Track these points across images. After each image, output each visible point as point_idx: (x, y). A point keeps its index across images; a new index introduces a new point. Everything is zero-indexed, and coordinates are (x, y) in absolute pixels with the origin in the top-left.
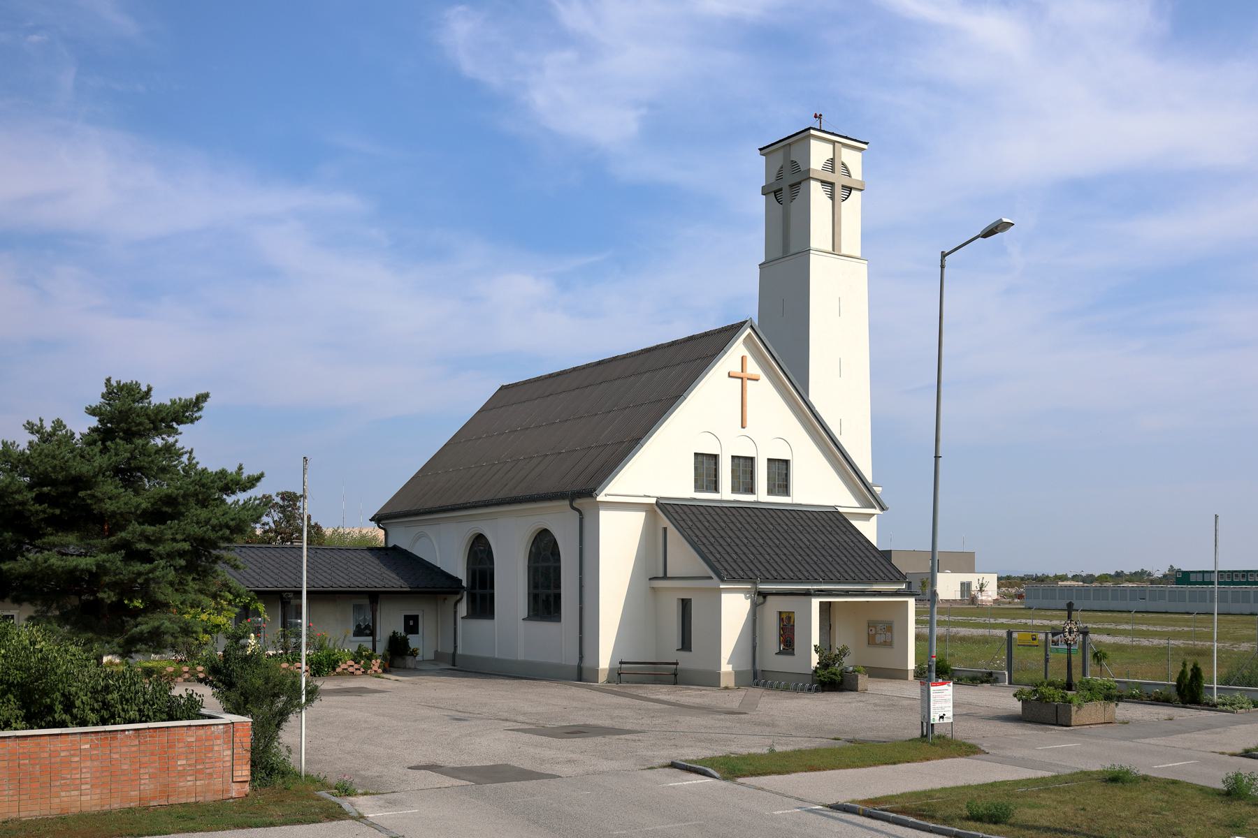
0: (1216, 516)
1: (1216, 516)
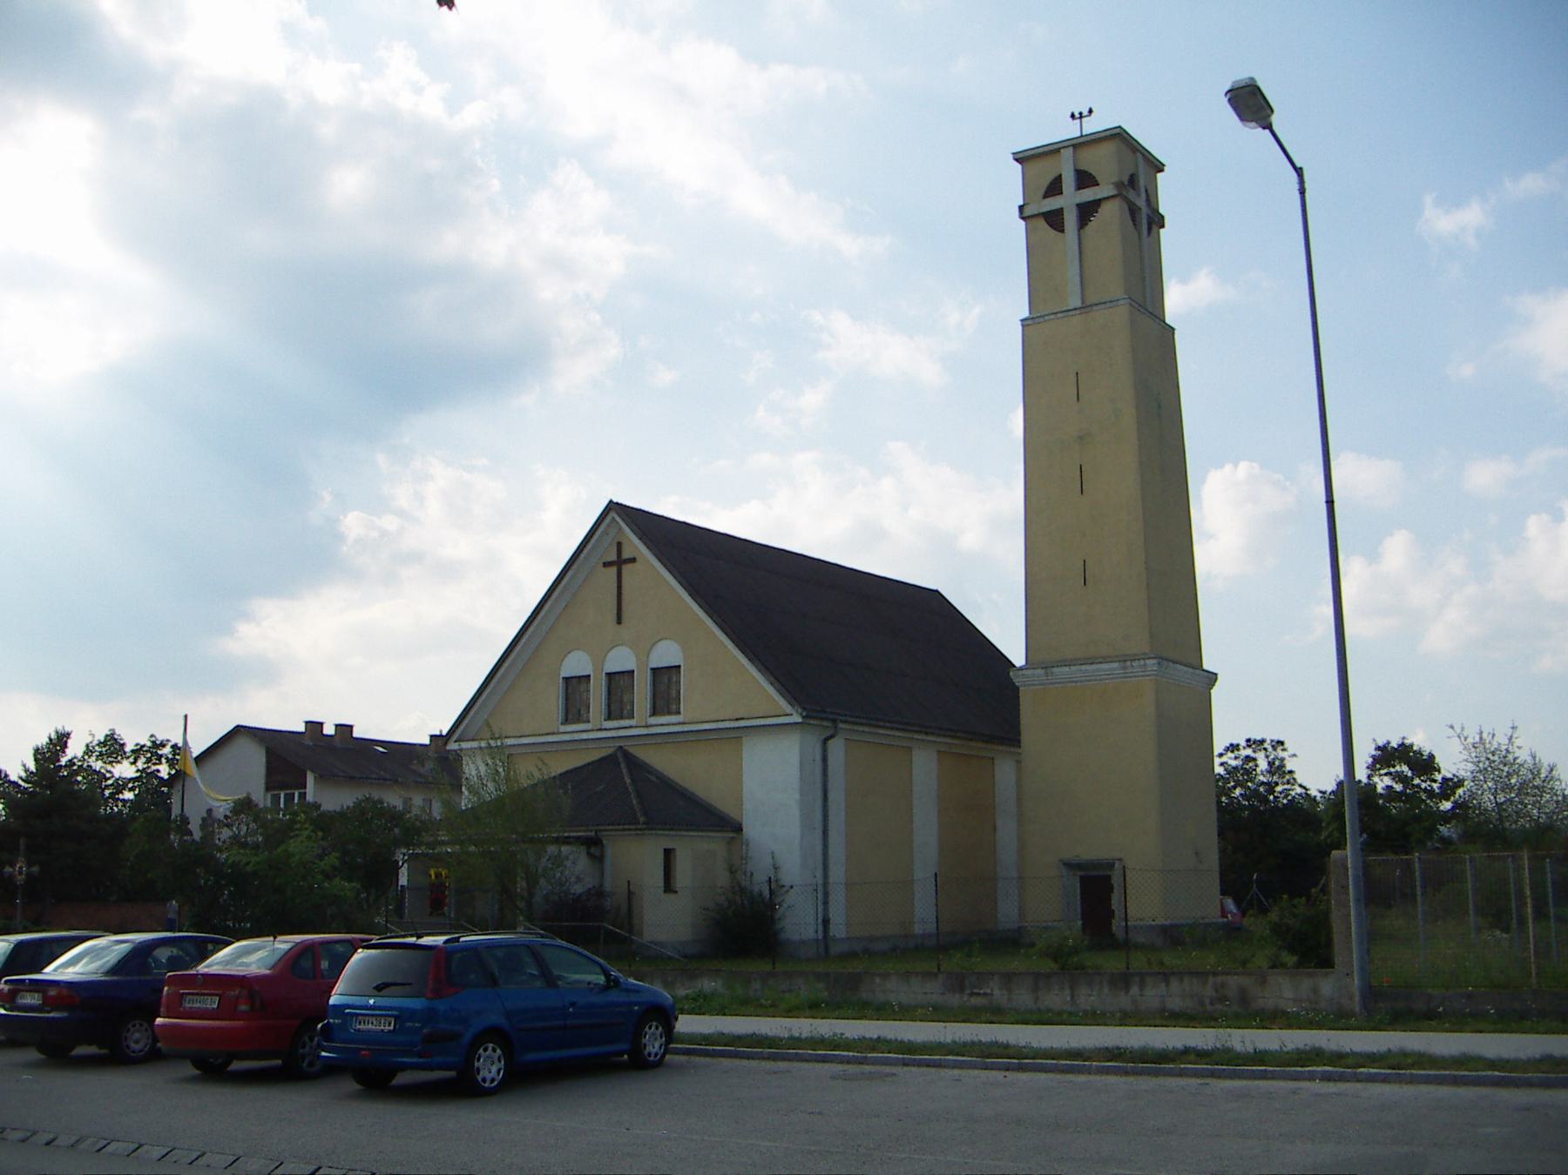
0: (619, 621)
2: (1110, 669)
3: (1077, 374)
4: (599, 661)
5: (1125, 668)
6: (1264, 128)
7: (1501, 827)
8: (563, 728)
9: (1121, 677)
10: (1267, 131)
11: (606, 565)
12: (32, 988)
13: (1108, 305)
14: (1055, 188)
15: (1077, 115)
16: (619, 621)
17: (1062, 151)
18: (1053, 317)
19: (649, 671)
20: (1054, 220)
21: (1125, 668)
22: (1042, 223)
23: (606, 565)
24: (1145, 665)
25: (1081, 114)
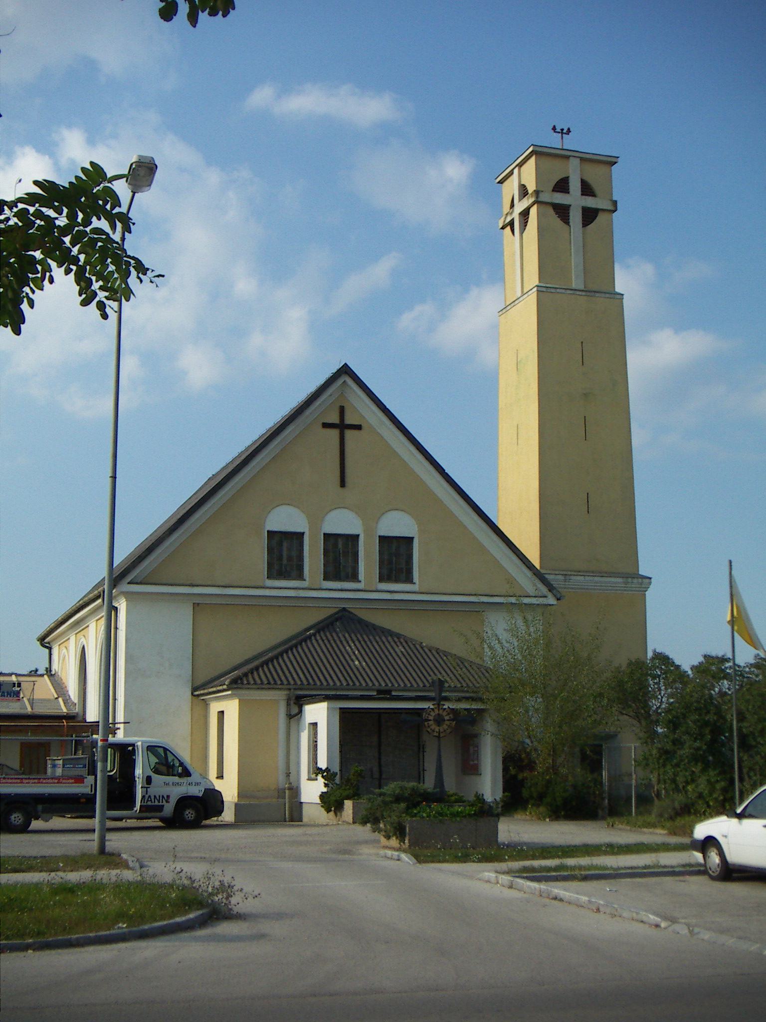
0: (343, 484)
2: (615, 583)
3: (582, 342)
4: (315, 520)
5: (626, 583)
6: (132, 191)
7: (172, 764)
8: (270, 583)
9: (622, 590)
10: (131, 194)
11: (326, 425)
12: (144, 815)
13: (607, 295)
14: (562, 186)
15: (558, 130)
16: (343, 484)
17: (571, 158)
18: (563, 291)
19: (378, 537)
20: (562, 212)
21: (626, 583)
22: (551, 211)
23: (326, 425)
24: (641, 584)
25: (562, 130)
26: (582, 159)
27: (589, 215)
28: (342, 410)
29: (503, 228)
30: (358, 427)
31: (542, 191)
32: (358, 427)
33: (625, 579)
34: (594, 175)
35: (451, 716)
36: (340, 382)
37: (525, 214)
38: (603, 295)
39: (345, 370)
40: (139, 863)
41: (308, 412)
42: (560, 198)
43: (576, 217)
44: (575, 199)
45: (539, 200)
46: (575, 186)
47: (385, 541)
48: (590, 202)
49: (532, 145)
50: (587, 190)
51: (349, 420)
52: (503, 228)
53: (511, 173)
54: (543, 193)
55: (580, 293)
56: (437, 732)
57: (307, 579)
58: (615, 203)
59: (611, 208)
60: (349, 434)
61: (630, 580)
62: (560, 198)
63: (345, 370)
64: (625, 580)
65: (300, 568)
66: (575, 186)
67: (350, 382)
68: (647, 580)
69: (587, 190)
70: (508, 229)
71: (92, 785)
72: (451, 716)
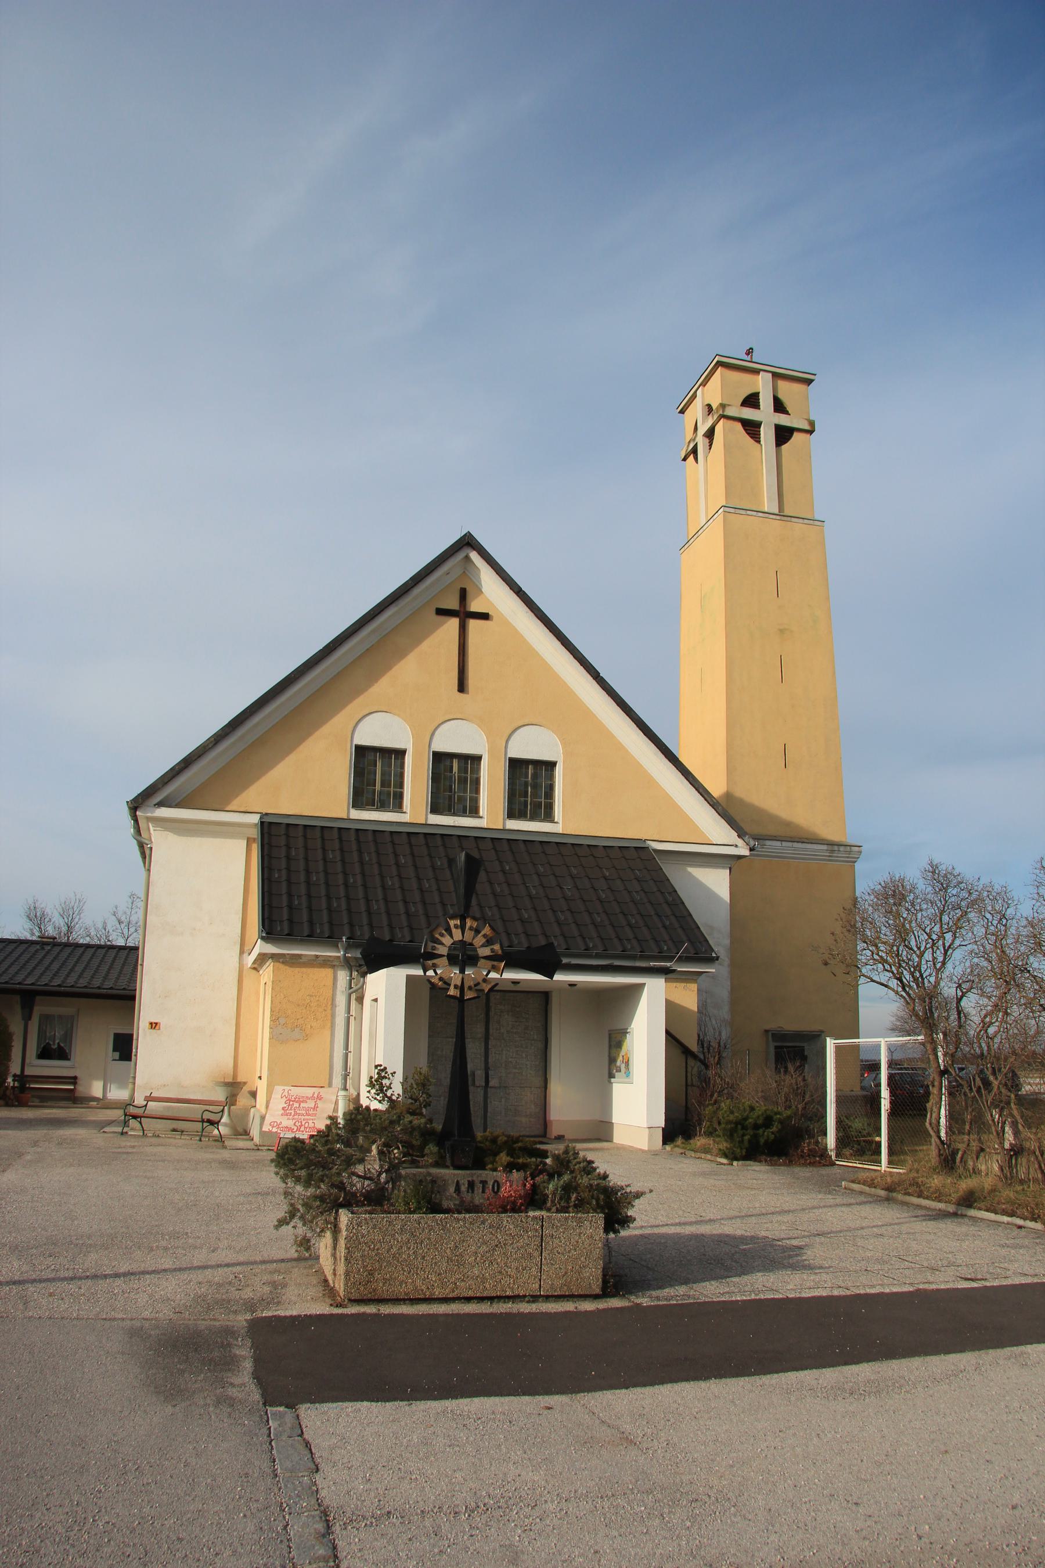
0: (462, 687)
1: (462, 687)
20: (752, 428)
21: (833, 851)
22: (738, 426)
26: (776, 376)
27: (783, 435)
28: (463, 594)
29: (685, 459)
30: (485, 616)
31: (729, 405)
32: (485, 616)
33: (830, 846)
34: (788, 391)
35: (497, 947)
36: (461, 555)
37: (710, 434)
38: (801, 521)
39: (467, 542)
40: (423, 1152)
41: (416, 591)
42: (748, 413)
43: (767, 434)
44: (766, 415)
45: (725, 414)
46: (766, 401)
47: (516, 765)
48: (783, 420)
49: (719, 364)
50: (779, 406)
51: (475, 606)
52: (685, 459)
53: (694, 396)
54: (730, 407)
55: (774, 517)
56: (456, 987)
57: (408, 812)
58: (812, 424)
59: (807, 427)
60: (473, 624)
61: (836, 848)
62: (748, 413)
63: (467, 542)
64: (830, 848)
65: (399, 797)
66: (766, 401)
67: (474, 556)
68: (856, 849)
69: (779, 406)
70: (691, 458)
71: (110, 1091)
72: (497, 947)
